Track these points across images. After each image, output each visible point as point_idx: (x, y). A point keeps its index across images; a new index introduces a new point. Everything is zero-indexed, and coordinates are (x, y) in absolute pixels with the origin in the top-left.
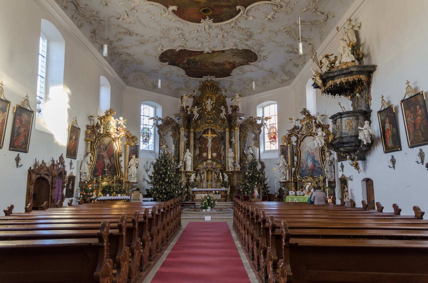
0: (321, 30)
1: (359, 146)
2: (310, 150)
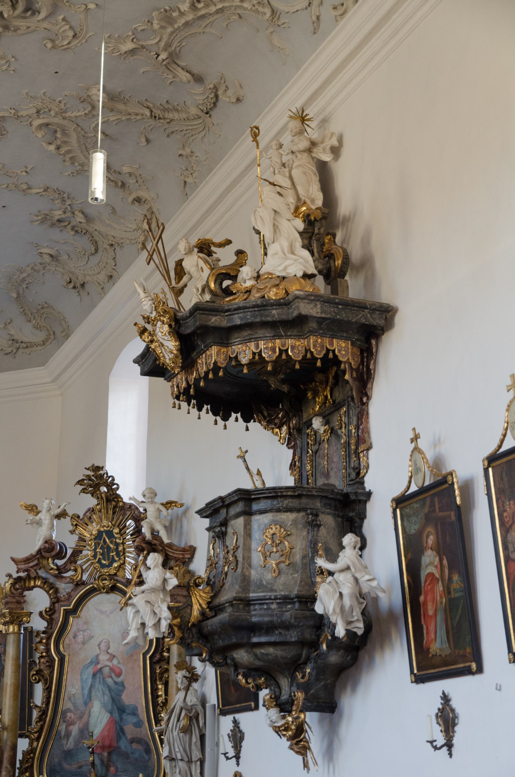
0: (188, 150)
1: (315, 645)
2: (104, 658)
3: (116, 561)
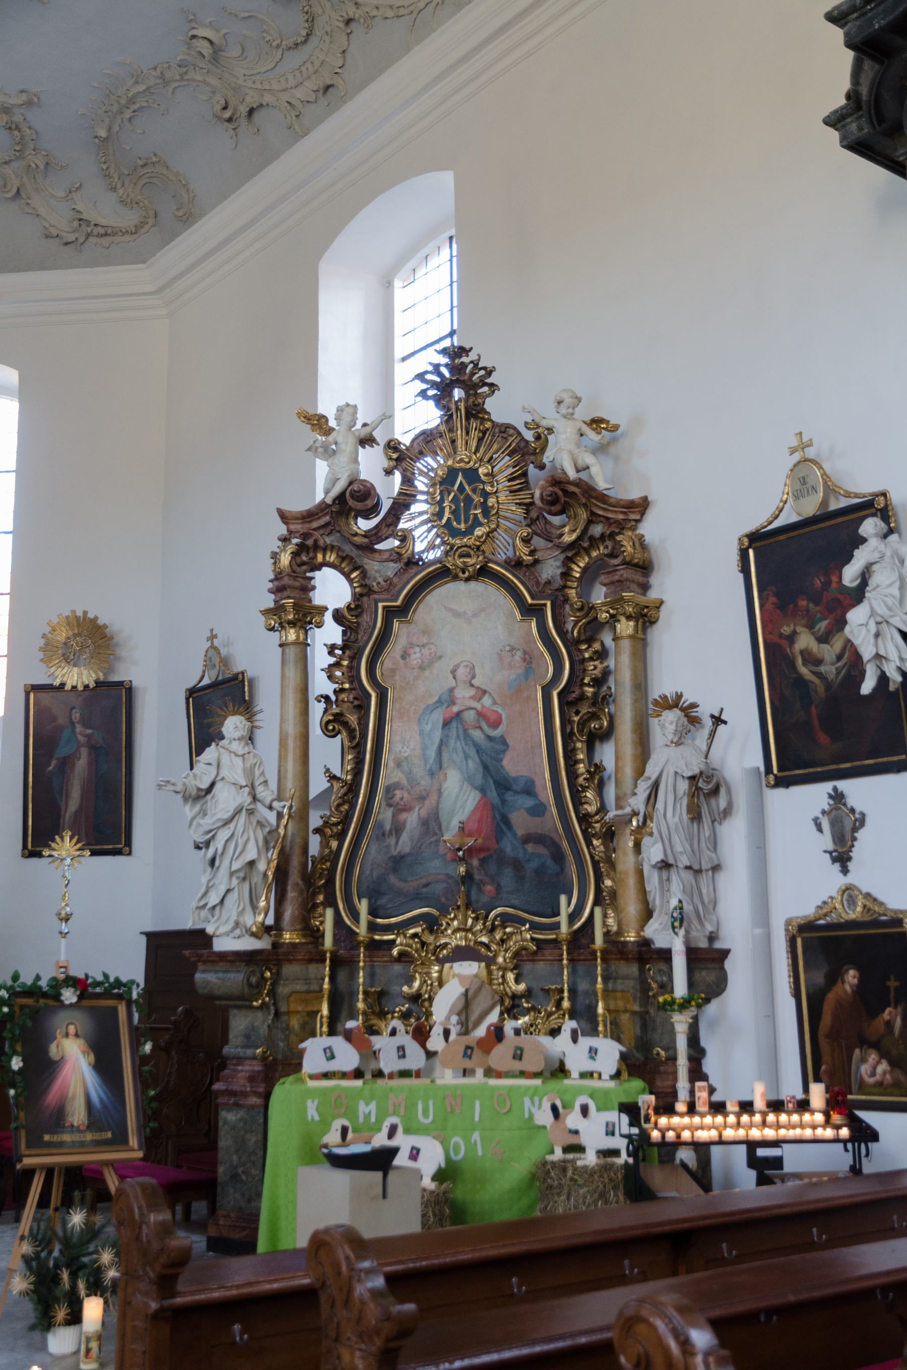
2: (464, 694)
3: (481, 525)
